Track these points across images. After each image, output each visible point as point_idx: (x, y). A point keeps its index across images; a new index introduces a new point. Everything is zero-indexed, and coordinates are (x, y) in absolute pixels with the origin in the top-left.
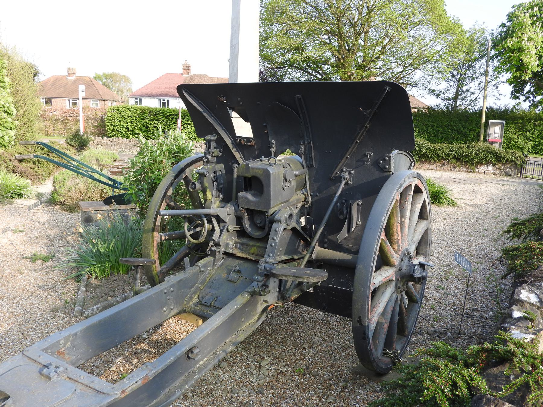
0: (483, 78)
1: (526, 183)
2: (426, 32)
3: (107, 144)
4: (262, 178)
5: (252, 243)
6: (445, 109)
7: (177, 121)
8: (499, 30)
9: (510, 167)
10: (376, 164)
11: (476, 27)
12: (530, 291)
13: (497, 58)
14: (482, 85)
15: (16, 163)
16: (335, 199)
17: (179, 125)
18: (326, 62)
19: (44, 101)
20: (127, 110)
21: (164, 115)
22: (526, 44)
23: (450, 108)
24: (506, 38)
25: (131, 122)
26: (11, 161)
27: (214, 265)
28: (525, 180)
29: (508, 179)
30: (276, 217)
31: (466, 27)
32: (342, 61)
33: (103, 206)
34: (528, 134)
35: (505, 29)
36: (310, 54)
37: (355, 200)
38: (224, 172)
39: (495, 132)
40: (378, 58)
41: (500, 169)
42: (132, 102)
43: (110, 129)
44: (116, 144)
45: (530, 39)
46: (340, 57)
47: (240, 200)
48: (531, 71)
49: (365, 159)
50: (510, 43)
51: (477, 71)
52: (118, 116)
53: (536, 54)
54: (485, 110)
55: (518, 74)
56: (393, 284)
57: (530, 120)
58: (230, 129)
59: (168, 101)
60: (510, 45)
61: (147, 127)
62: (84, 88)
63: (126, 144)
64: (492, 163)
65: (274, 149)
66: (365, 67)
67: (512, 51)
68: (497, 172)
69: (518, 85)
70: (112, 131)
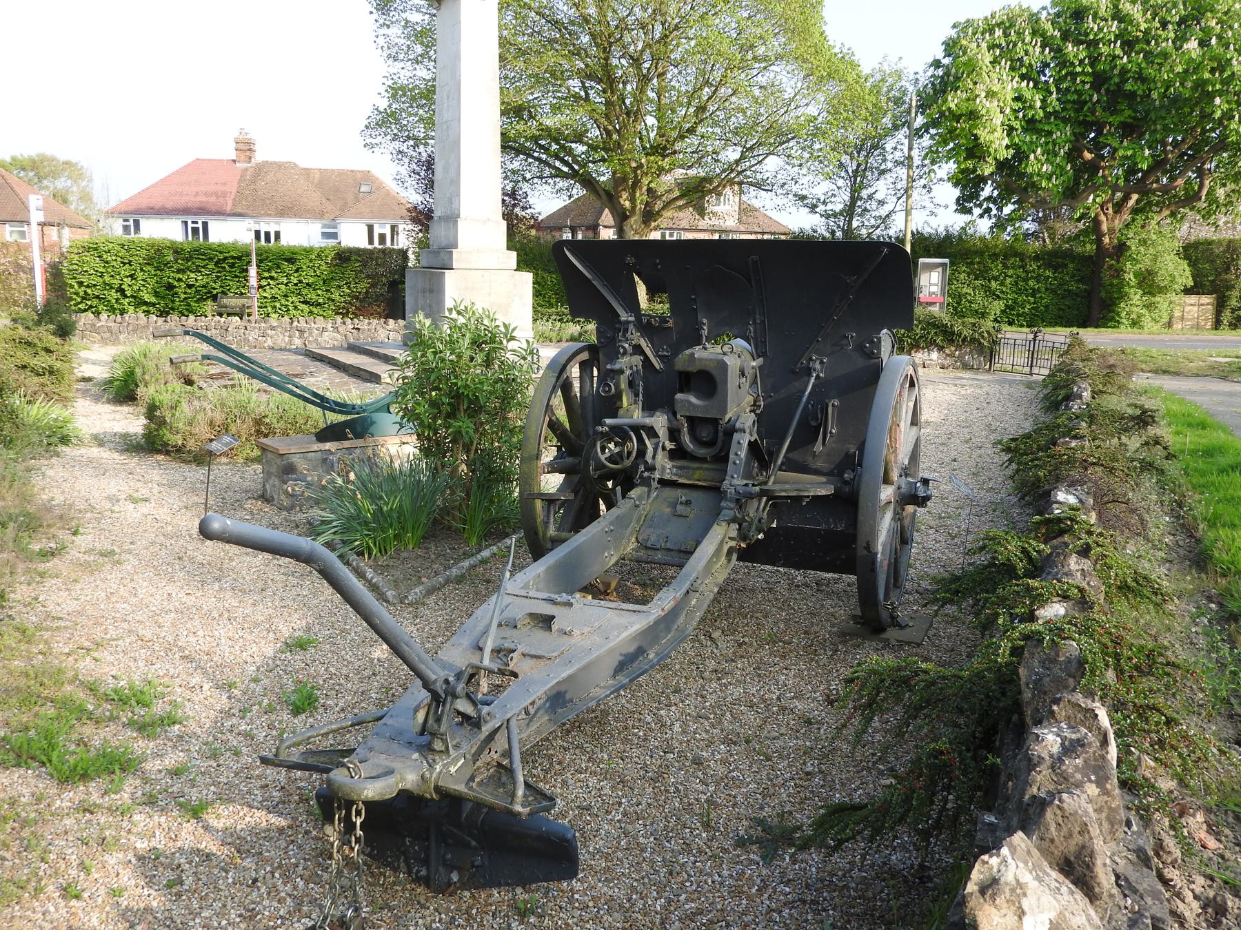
0: (902, 172)
1: (1002, 382)
2: (786, 78)
3: (109, 330)
4: (714, 372)
5: (696, 465)
6: (828, 235)
8: (929, 73)
9: (971, 352)
10: (860, 348)
11: (885, 67)
12: (1068, 492)
13: (927, 131)
14: (902, 184)
16: (804, 399)
17: (253, 281)
18: (579, 139)
20: (119, 248)
21: (211, 259)
22: (986, 106)
23: (839, 234)
24: (944, 92)
25: (131, 276)
27: (649, 496)
28: (998, 376)
29: (968, 374)
30: (737, 425)
31: (866, 69)
32: (615, 136)
33: (312, 443)
34: (994, 285)
35: (940, 72)
36: (549, 122)
37: (830, 399)
38: (640, 367)
39: (930, 282)
40: (692, 131)
41: (952, 356)
42: (116, 228)
43: (77, 294)
44: (130, 328)
45: (990, 94)
46: (610, 128)
47: (678, 407)
48: (996, 159)
49: (844, 342)
50: (953, 101)
51: (889, 157)
53: (1003, 124)
54: (909, 236)
55: (970, 164)
56: (892, 506)
57: (994, 256)
59: (205, 225)
60: (952, 105)
61: (170, 287)
62: (40, 203)
64: (937, 345)
66: (665, 148)
67: (957, 118)
68: (946, 362)
69: (969, 186)
70: (83, 298)
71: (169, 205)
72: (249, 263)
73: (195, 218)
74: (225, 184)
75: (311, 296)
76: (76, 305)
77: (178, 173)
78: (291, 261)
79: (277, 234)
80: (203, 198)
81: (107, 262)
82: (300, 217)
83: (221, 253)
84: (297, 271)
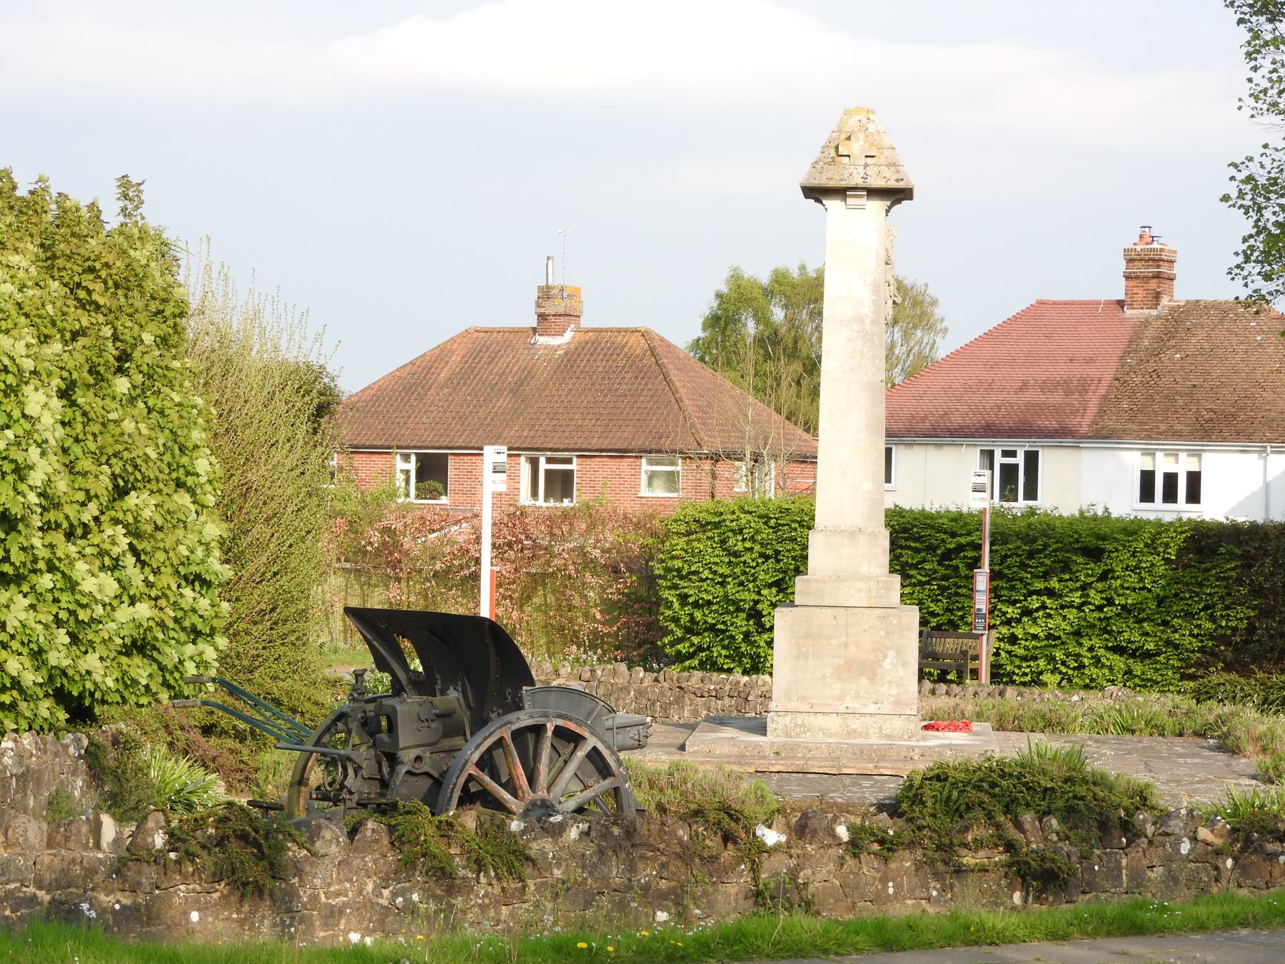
7: (971, 578)
15: (196, 735)
17: (981, 602)
19: (412, 466)
21: (932, 549)
26: (182, 728)
43: (676, 620)
52: (713, 554)
58: (405, 666)
59: (1032, 459)
63: (640, 693)
65: (438, 687)
71: (956, 420)
72: (975, 563)
73: (1009, 444)
74: (1090, 361)
75: (1130, 635)
76: (672, 644)
77: (991, 337)
78: (1095, 554)
79: (1194, 480)
80: (1033, 396)
81: (736, 554)
82: (1249, 438)
83: (953, 535)
84: (1103, 577)
